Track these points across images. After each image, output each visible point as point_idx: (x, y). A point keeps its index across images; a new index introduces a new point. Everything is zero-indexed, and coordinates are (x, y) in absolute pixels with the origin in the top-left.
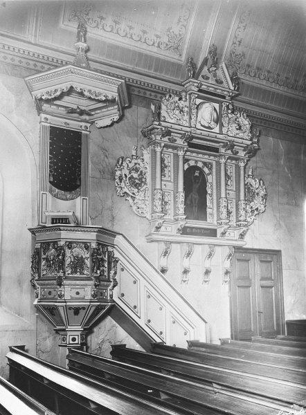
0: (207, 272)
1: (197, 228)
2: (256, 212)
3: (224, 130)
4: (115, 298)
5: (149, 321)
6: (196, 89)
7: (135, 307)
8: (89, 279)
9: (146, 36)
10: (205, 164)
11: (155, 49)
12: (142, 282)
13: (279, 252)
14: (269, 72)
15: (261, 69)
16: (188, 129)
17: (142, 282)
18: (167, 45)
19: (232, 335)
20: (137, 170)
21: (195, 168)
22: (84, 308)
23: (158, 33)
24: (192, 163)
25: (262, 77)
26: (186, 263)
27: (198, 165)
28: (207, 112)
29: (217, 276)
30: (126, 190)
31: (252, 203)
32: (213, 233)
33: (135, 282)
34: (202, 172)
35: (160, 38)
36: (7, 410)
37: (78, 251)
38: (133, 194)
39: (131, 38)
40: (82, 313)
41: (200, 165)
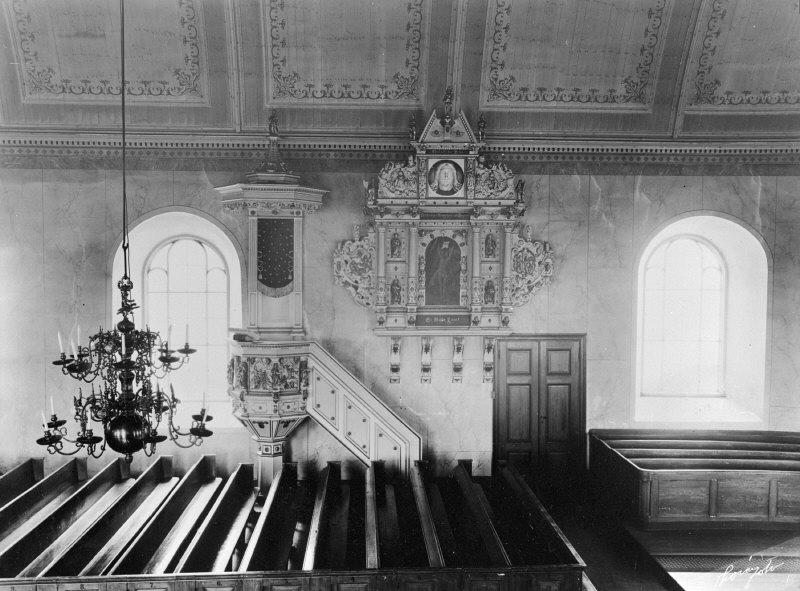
0: (457, 369)
3: (471, 195)
4: (310, 409)
5: (350, 434)
7: (333, 419)
8: (269, 394)
11: (382, 101)
12: (341, 392)
13: (583, 336)
15: (545, 90)
17: (341, 392)
21: (442, 240)
22: (294, 421)
24: (437, 234)
26: (426, 358)
28: (447, 176)
29: (473, 371)
30: (346, 278)
31: (529, 277)
32: (467, 321)
33: (333, 392)
34: (452, 243)
35: (408, 60)
36: (494, 441)
37: (261, 366)
38: (356, 282)
39: (350, 96)
40: (291, 424)
41: (449, 234)
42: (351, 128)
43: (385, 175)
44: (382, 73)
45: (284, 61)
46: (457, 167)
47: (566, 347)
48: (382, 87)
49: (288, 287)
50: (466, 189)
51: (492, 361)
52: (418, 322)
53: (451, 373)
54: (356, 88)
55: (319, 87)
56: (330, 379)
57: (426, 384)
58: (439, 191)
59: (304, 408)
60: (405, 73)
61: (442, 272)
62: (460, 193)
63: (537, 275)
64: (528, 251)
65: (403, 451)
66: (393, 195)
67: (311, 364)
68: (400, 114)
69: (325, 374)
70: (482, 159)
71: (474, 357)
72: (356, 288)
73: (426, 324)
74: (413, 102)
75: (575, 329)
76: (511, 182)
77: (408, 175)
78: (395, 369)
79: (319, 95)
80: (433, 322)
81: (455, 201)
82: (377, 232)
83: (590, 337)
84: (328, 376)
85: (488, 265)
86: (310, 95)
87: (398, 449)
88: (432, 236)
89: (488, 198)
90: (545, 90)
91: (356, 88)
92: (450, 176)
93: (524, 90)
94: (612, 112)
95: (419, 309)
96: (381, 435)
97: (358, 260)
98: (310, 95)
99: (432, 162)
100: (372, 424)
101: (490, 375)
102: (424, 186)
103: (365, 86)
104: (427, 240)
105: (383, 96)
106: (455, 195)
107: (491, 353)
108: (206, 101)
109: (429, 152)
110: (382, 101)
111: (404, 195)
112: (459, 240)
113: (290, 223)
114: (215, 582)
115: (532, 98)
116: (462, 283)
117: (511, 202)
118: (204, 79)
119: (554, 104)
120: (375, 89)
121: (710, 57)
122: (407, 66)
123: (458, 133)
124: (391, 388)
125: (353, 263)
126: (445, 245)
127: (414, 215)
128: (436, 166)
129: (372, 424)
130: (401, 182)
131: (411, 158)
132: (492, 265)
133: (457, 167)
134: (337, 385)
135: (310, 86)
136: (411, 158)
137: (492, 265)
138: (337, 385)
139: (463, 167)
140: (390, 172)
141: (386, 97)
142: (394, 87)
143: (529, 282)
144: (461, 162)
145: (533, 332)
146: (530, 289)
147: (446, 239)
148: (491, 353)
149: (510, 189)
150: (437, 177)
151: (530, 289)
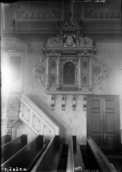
0: (74, 106)
1: (68, 88)
2: (101, 79)
3: (78, 46)
6: (62, 32)
9: (28, 16)
10: (74, 60)
14: (107, 14)
16: (59, 48)
18: (54, 17)
19: (87, 135)
20: (42, 67)
21: (69, 63)
22: (14, 120)
23: (50, 14)
24: (67, 61)
25: (104, 17)
27: (64, 64)
28: (70, 40)
31: (98, 75)
32: (76, 89)
33: (39, 121)
36: (87, 132)
39: (39, 18)
40: (13, 121)
41: (71, 61)
43: (49, 40)
46: (73, 37)
47: (113, 112)
48: (50, 15)
50: (76, 44)
51: (86, 103)
52: (60, 89)
53: (72, 108)
56: (49, 127)
57: (63, 111)
58: (67, 45)
59: (18, 116)
61: (68, 72)
62: (74, 46)
63: (101, 75)
64: (98, 66)
65: (51, 131)
66: (52, 47)
67: (22, 101)
69: (47, 125)
70: (82, 35)
71: (81, 103)
73: (63, 90)
76: (91, 42)
77: (56, 40)
78: (53, 106)
79: (30, 18)
80: (66, 89)
81: (73, 48)
84: (48, 126)
85: (84, 71)
86: (27, 18)
87: (51, 132)
88: (65, 62)
89: (84, 47)
90: (102, 14)
92: (71, 40)
93: (96, 14)
95: (61, 85)
96: (45, 127)
97: (41, 69)
98: (27, 18)
99: (65, 36)
100: (31, 113)
101: (85, 109)
102: (62, 43)
104: (64, 63)
105: (50, 18)
106: (72, 47)
107: (86, 101)
111: (55, 46)
115: (98, 17)
117: (92, 48)
119: (106, 19)
122: (57, 7)
123: (73, 26)
124: (51, 112)
125: (39, 70)
126: (70, 65)
127: (58, 53)
128: (66, 37)
129: (31, 113)
130: (54, 42)
131: (58, 35)
132: (86, 71)
133: (73, 37)
134: (30, 108)
136: (58, 35)
137: (86, 71)
138: (30, 108)
139: (75, 38)
140: (51, 39)
141: (51, 18)
143: (99, 77)
144: (74, 36)
145: (100, 94)
146: (99, 79)
147: (71, 63)
148: (86, 101)
150: (67, 41)
151: (99, 79)
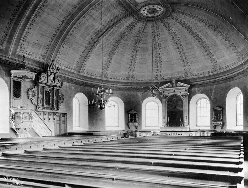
11: (38, 59)
13: (67, 113)
34: (49, 92)
41: (48, 90)
42: (81, 78)
44: (40, 53)
45: (23, 44)
49: (19, 98)
54: (34, 55)
55: (28, 52)
60: (44, 54)
68: (41, 63)
72: (33, 100)
74: (43, 61)
75: (66, 113)
82: (38, 88)
83: (67, 114)
91: (34, 55)
94: (107, 83)
97: (33, 93)
103: (36, 55)
108: (4, 48)
109: (50, 72)
110: (38, 59)
112: (50, 92)
113: (20, 82)
114: (173, 91)
116: (50, 101)
118: (5, 43)
120: (38, 56)
121: (8, 27)
125: (32, 94)
135: (26, 52)
142: (41, 57)
149: (61, 82)
